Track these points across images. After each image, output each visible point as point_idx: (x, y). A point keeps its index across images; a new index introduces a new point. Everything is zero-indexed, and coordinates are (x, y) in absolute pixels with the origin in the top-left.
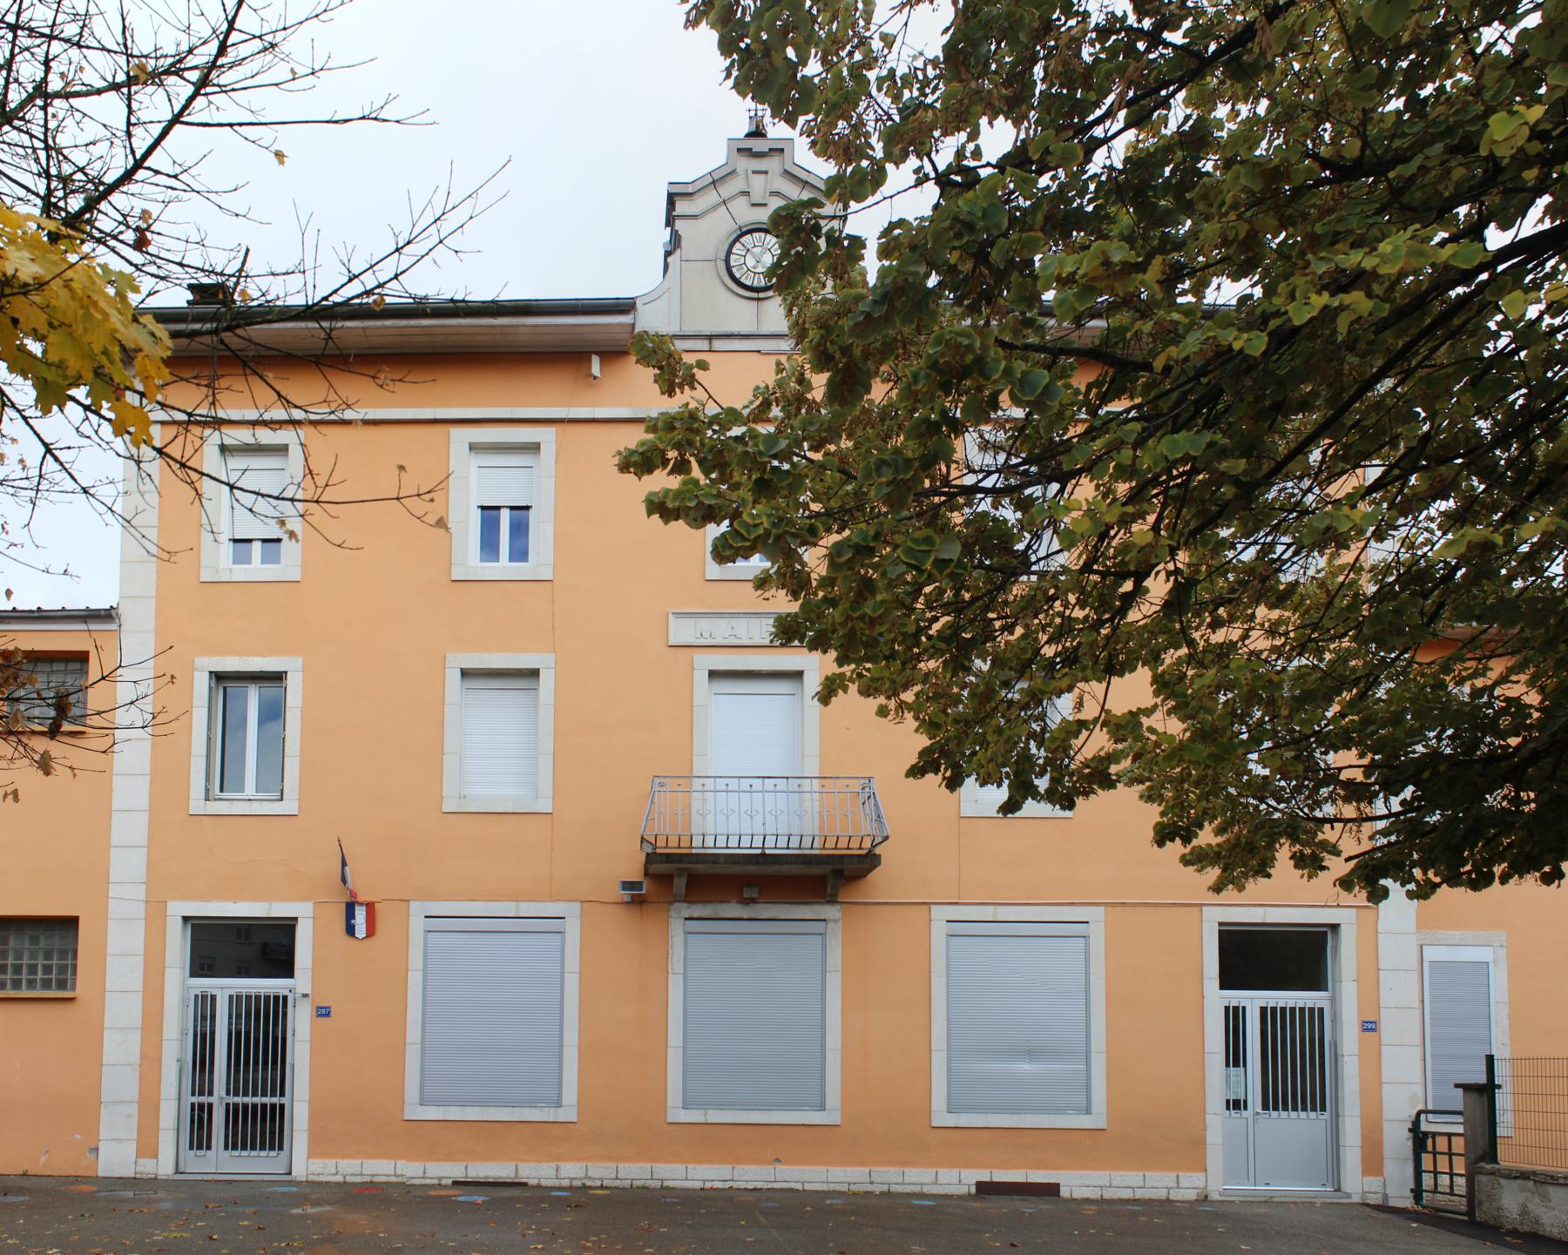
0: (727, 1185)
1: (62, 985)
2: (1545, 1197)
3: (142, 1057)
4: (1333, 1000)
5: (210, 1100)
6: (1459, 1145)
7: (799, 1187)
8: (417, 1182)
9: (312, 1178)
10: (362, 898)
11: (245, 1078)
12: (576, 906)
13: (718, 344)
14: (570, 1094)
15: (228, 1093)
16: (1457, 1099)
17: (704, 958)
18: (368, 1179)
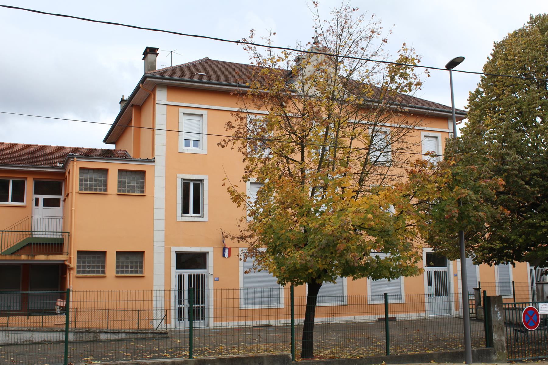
4: (448, 269)
10: (227, 246)
11: (193, 298)
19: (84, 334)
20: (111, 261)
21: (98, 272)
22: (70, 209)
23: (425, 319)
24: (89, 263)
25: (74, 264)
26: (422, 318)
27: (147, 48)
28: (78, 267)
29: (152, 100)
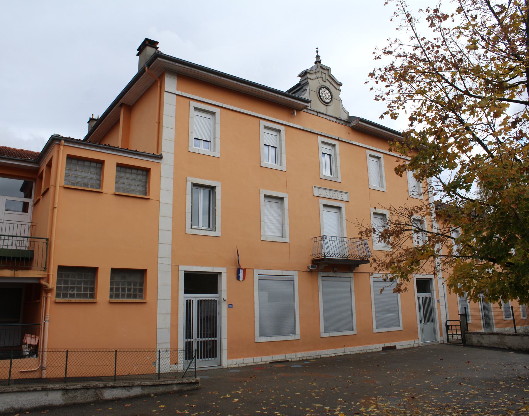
0: (335, 355)
1: (141, 297)
2: (483, 338)
3: (171, 325)
5: (192, 340)
6: (459, 328)
7: (349, 353)
8: (260, 363)
9: (229, 366)
12: (297, 272)
13: (319, 115)
14: (298, 331)
15: (198, 337)
16: (459, 318)
17: (327, 288)
18: (246, 365)
19: (79, 392)
20: (104, 281)
21: (85, 296)
22: (50, 207)
23: (419, 346)
24: (73, 283)
25: (52, 284)
26: (416, 345)
27: (146, 40)
28: (58, 288)
29: (159, 88)
